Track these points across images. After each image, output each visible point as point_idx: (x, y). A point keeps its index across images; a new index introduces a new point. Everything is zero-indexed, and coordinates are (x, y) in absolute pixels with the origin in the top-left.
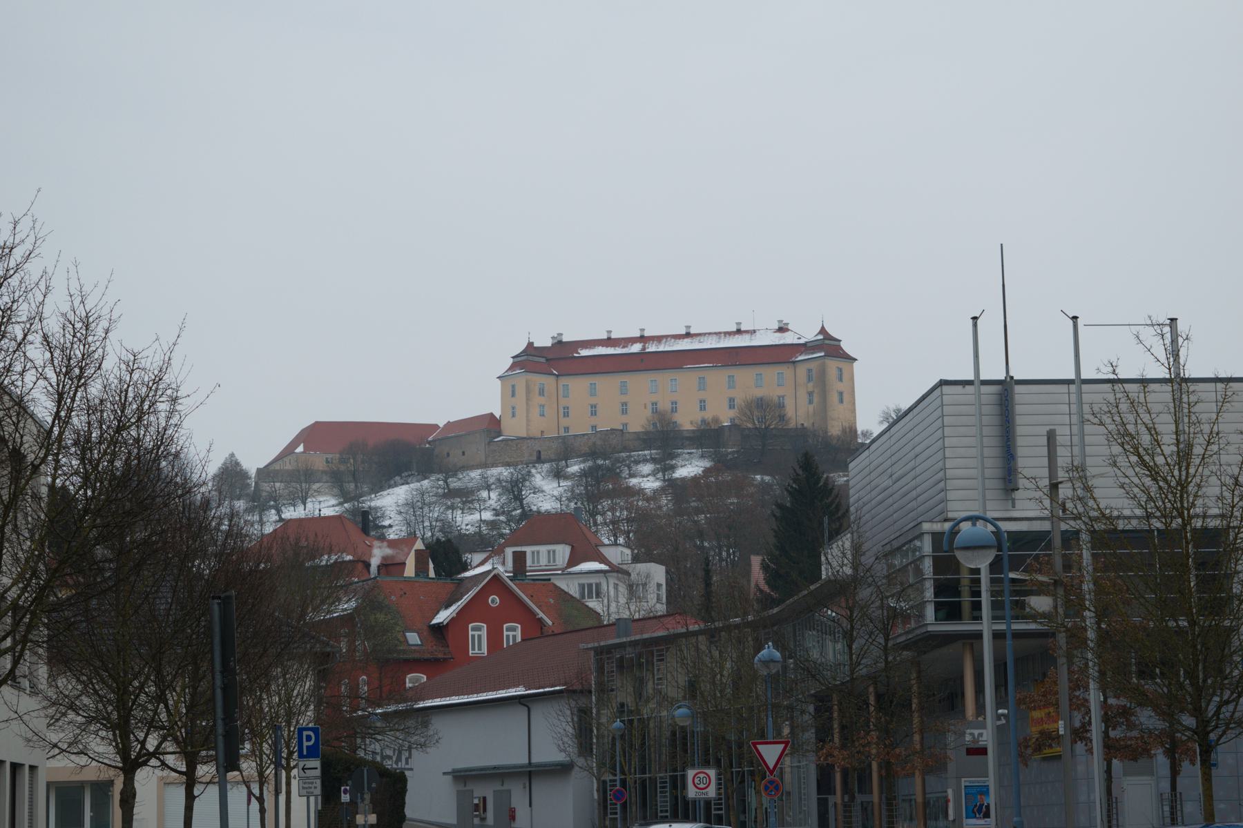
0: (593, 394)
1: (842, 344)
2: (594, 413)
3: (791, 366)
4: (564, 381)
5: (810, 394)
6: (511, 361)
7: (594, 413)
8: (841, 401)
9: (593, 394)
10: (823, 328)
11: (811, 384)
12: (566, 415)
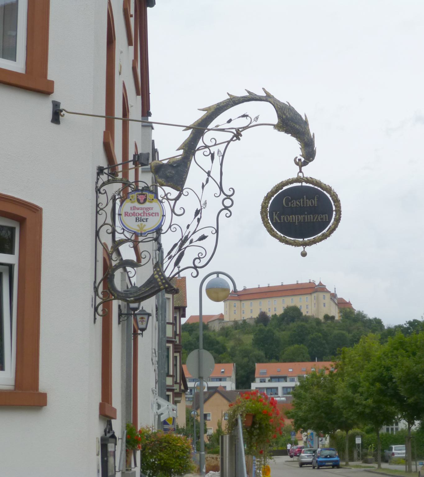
0: (251, 306)
1: (327, 287)
2: (251, 312)
5: (315, 304)
7: (251, 312)
8: (324, 306)
9: (251, 306)
10: (320, 282)
12: (243, 313)
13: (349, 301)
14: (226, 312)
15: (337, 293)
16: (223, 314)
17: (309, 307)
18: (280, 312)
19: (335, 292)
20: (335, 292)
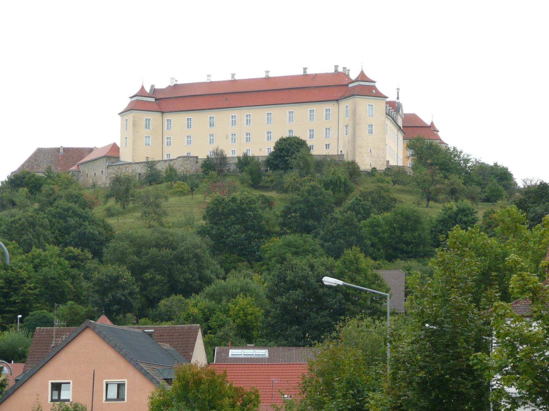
3: (335, 103)
4: (167, 117)
6: (129, 101)
8: (371, 132)
11: (347, 118)
13: (432, 123)
14: (125, 139)
15: (401, 101)
16: (119, 144)
17: (333, 134)
18: (262, 148)
19: (398, 98)
20: (398, 98)
